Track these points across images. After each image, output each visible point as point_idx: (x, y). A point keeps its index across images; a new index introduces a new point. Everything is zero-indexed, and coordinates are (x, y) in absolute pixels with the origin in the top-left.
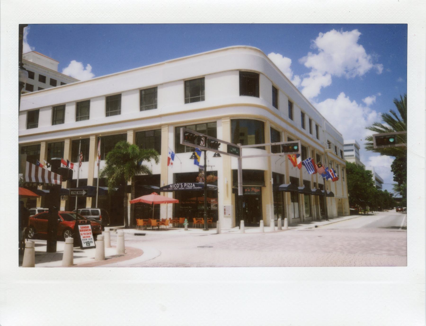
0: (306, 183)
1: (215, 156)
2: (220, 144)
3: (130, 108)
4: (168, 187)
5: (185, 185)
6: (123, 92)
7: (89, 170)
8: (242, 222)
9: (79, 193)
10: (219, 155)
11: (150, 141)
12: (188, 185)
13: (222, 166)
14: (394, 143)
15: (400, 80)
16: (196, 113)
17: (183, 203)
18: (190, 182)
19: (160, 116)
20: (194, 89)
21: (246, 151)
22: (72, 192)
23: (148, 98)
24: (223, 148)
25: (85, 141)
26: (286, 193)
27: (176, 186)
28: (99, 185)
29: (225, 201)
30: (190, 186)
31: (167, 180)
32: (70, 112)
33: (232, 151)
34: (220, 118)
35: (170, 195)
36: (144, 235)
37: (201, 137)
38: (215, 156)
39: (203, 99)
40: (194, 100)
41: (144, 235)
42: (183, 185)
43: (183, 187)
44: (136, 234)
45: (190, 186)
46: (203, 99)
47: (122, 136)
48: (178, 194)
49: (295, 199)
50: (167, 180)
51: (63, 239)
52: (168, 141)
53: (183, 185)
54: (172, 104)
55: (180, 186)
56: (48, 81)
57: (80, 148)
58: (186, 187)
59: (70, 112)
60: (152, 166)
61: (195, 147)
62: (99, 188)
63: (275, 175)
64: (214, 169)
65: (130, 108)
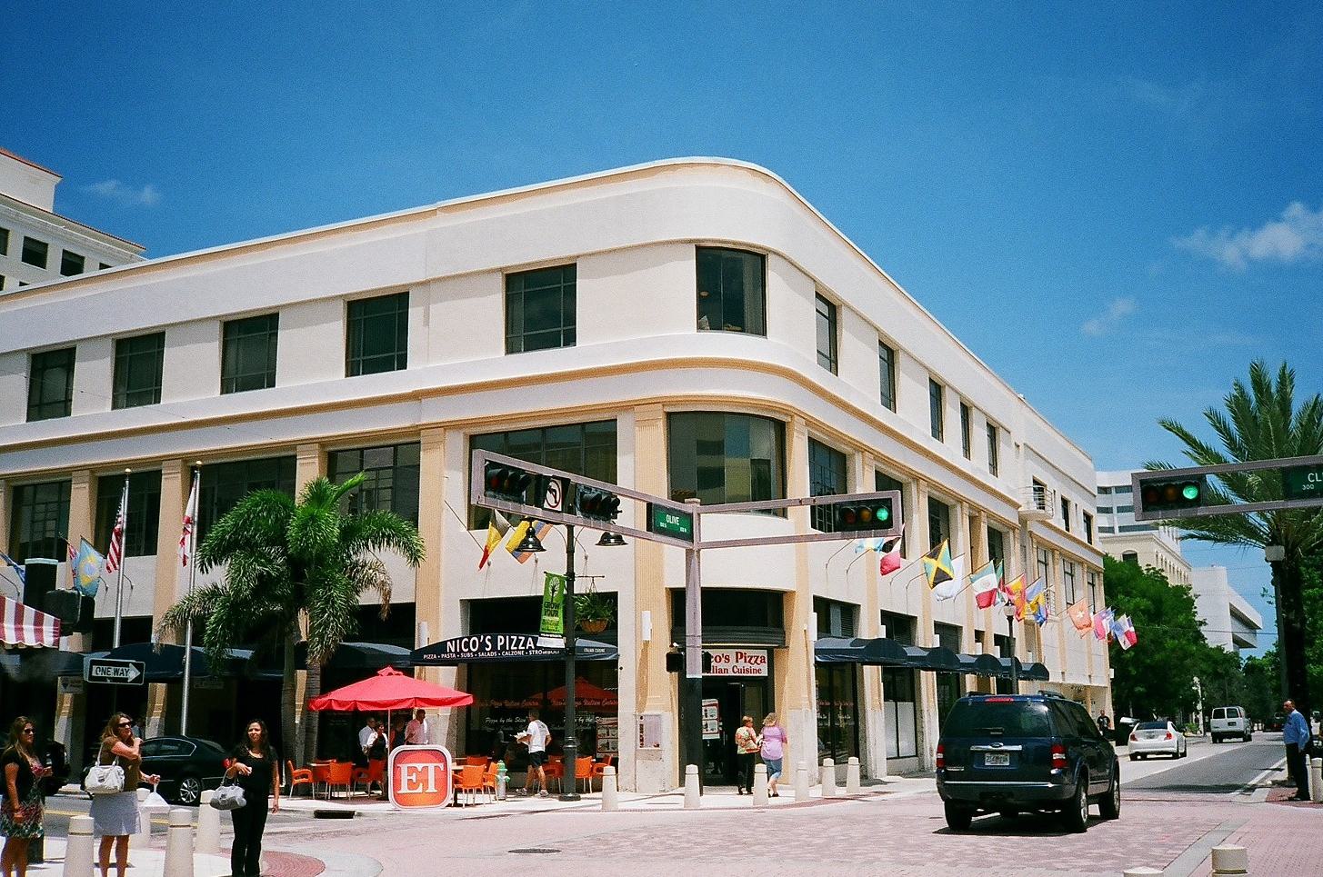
0: (948, 632)
1: (605, 540)
2: (618, 502)
3: (312, 368)
4: (440, 647)
5: (500, 644)
6: (284, 306)
7: (164, 582)
8: (693, 770)
9: (116, 671)
10: (619, 540)
11: (380, 482)
12: (511, 641)
13: (637, 573)
14: (1196, 502)
15: (704, 294)
16: (546, 385)
17: (497, 705)
18: (518, 631)
19: (416, 396)
20: (541, 305)
21: (714, 524)
22: (95, 667)
23: (377, 331)
24: (630, 515)
25: (146, 483)
26: (866, 668)
27: (467, 645)
28: (193, 644)
29: (646, 700)
30: (513, 645)
31: (441, 624)
32: (93, 378)
33: (662, 525)
34: (627, 407)
35: (444, 679)
36: (349, 815)
37: (548, 479)
38: (605, 540)
39: (570, 339)
40: (534, 344)
41: (349, 815)
42: (494, 641)
43: (494, 648)
44: (320, 815)
45: (517, 645)
46: (570, 339)
47: (278, 467)
48: (476, 674)
49: (900, 688)
50: (441, 624)
51: (245, 795)
52: (446, 484)
53: (494, 641)
54: (462, 357)
55: (483, 646)
56: (54, 259)
57: (129, 503)
58: (503, 647)
59: (93, 378)
60: (388, 572)
61: (527, 510)
62: (192, 651)
63: (822, 605)
64: (602, 587)
65: (312, 368)
